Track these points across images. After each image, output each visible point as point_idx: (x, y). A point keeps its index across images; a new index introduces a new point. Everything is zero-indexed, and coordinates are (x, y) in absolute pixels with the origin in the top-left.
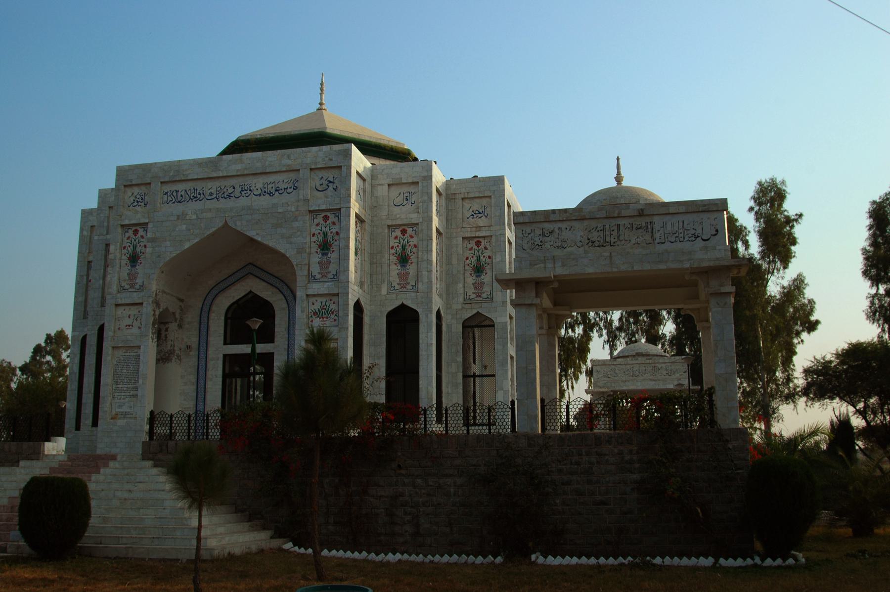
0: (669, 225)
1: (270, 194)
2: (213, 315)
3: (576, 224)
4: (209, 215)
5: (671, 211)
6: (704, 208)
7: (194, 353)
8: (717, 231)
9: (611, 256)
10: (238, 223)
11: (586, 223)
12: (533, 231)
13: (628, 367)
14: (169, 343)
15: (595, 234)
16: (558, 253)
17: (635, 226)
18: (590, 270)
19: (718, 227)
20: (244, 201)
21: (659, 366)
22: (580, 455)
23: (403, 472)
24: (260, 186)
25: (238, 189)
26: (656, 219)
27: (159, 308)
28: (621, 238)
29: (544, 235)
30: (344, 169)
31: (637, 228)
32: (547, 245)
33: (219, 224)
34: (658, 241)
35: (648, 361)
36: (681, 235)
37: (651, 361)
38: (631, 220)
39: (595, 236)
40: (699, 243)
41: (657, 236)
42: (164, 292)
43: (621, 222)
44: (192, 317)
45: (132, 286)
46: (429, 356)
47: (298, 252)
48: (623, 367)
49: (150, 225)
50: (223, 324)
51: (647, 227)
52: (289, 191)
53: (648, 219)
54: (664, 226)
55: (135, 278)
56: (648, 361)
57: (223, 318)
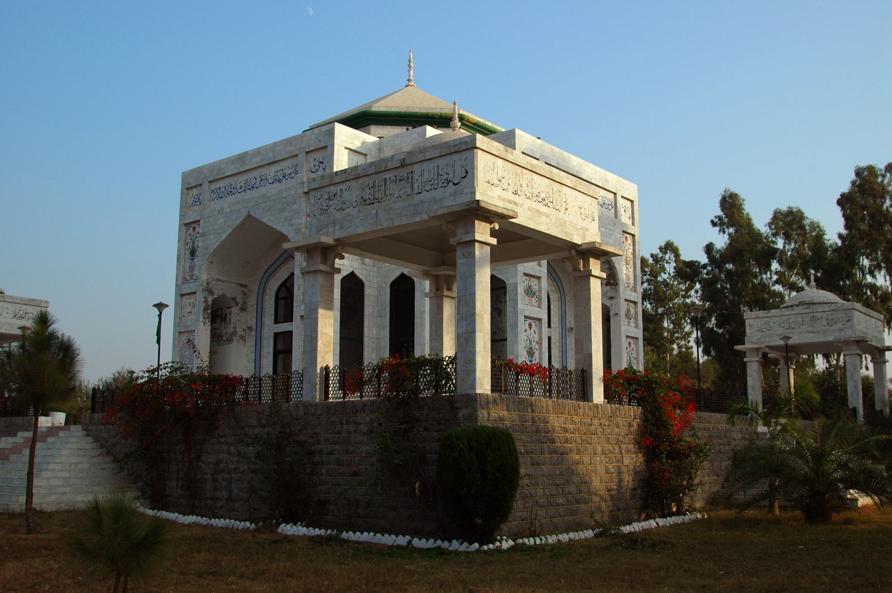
0: (426, 171)
1: (280, 181)
2: (267, 297)
3: (353, 184)
4: (238, 207)
5: (427, 157)
6: (456, 149)
7: (254, 333)
8: (467, 172)
9: (377, 214)
10: (257, 212)
11: (361, 181)
12: (322, 196)
13: (784, 318)
14: (232, 325)
15: (368, 191)
16: (339, 215)
17: (398, 178)
18: (360, 230)
19: (468, 168)
20: (262, 191)
21: (818, 315)
22: (342, 424)
23: (222, 440)
24: (273, 174)
25: (259, 180)
26: (416, 168)
27: (212, 295)
28: (387, 193)
29: (329, 199)
30: (329, 148)
31: (400, 180)
32: (331, 209)
33: (244, 214)
34: (416, 191)
35: (805, 311)
36: (436, 182)
37: (808, 311)
38: (394, 173)
39: (367, 194)
40: (451, 188)
41: (416, 185)
42: (218, 280)
43: (388, 175)
44: (252, 300)
45: (192, 278)
46: (423, 323)
47: (296, 233)
48: (778, 319)
49: (201, 222)
50: (273, 305)
51: (408, 177)
52: (292, 175)
53: (409, 169)
54: (423, 171)
55: (194, 270)
56: (805, 311)
57: (273, 299)
